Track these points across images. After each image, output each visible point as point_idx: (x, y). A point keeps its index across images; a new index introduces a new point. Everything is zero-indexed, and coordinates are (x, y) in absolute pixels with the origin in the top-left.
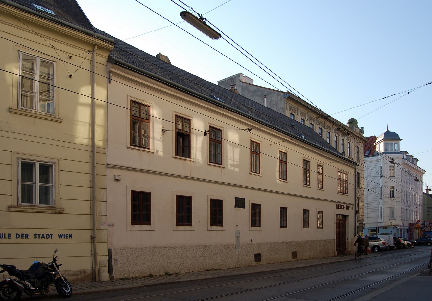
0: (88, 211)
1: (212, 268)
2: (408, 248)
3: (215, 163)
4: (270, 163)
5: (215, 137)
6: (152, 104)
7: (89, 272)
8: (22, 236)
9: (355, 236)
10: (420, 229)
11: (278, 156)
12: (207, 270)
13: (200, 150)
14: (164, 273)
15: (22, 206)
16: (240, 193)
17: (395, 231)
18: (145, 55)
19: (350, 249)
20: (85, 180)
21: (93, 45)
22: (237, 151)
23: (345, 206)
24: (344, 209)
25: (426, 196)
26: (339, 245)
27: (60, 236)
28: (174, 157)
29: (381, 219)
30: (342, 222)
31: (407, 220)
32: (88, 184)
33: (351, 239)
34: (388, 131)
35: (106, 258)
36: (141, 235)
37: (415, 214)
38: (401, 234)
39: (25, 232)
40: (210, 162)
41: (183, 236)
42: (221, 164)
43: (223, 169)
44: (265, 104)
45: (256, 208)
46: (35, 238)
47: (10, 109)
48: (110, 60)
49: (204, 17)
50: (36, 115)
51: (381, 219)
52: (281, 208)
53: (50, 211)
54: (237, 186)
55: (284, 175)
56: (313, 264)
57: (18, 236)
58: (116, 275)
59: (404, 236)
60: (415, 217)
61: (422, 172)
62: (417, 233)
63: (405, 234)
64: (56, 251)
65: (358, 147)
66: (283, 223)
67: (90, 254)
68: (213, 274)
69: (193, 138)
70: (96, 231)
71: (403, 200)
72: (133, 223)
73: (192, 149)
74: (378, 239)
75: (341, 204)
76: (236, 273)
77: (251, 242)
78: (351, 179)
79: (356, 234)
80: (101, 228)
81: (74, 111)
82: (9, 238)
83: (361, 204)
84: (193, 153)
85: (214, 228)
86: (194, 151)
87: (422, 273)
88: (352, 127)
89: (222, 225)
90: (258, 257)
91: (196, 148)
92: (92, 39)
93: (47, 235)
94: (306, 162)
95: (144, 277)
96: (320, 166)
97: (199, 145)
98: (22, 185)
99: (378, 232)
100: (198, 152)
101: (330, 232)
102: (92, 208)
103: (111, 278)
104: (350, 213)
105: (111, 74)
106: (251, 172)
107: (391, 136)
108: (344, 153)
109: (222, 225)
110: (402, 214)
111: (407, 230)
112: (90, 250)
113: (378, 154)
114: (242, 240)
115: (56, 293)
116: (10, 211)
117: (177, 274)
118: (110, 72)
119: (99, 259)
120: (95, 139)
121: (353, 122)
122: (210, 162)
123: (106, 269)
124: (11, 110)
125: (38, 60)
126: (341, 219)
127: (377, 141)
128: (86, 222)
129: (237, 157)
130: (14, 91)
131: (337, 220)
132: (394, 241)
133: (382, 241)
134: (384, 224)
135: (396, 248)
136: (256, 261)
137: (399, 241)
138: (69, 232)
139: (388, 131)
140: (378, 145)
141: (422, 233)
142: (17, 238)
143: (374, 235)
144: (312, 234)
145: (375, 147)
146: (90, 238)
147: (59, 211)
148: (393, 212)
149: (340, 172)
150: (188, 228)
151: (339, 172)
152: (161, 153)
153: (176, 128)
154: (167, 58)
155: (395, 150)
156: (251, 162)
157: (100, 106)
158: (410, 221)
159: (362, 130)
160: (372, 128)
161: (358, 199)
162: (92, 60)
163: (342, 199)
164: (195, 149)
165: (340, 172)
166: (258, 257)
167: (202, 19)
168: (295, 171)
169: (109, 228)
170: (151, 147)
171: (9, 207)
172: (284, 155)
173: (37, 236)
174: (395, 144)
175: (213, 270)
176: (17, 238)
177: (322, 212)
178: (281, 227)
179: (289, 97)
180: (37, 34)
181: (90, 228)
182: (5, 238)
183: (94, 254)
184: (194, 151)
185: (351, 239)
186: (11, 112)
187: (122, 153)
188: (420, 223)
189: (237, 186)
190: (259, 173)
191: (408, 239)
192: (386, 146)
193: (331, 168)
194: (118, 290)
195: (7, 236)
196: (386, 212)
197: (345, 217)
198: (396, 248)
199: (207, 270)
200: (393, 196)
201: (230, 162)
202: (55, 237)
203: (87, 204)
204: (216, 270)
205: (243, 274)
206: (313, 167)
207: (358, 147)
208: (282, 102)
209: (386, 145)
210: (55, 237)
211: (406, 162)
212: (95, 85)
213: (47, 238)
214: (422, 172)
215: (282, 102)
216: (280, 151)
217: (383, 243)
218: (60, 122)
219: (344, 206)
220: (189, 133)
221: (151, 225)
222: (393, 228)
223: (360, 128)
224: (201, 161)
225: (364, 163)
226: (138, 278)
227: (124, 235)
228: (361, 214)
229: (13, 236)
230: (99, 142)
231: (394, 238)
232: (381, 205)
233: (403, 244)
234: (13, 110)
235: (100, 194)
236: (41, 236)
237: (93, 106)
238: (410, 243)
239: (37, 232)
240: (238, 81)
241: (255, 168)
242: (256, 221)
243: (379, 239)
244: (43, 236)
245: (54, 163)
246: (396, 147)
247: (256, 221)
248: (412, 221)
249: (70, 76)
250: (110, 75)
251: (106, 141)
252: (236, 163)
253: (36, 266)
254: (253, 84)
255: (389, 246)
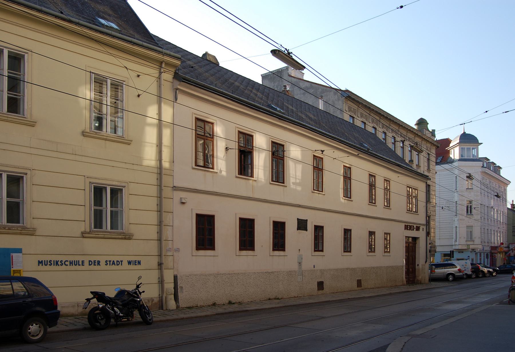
0: (155, 236)
1: (274, 297)
2: (489, 277)
3: (278, 182)
4: (333, 180)
5: (278, 153)
6: (216, 120)
7: (156, 300)
8: (94, 263)
9: (426, 262)
10: (504, 254)
11: (342, 172)
12: (269, 299)
13: (262, 168)
14: (227, 302)
15: (95, 232)
16: (303, 214)
17: (473, 256)
18: (195, 58)
19: (420, 277)
20: (153, 203)
21: (161, 63)
22: (300, 167)
23: (415, 227)
24: (413, 230)
25: (511, 212)
26: (407, 273)
27: (129, 263)
28: (237, 177)
29: (456, 241)
30: (411, 246)
31: (488, 243)
32: (155, 208)
33: (422, 265)
34: (464, 133)
35: (172, 285)
36: (204, 262)
37: (497, 234)
38: (480, 259)
39: (97, 258)
40: (272, 181)
41: (246, 262)
42: (283, 183)
43: (285, 188)
44: (321, 106)
45: (319, 230)
46: (106, 265)
47: (83, 132)
48: (177, 76)
49: (290, 51)
50: (108, 138)
51: (456, 241)
52: (345, 229)
53: (120, 237)
54: (299, 206)
55: (348, 193)
56: (381, 294)
57: (91, 263)
58: (182, 304)
59: (484, 262)
60: (497, 238)
61: (506, 183)
62: (500, 258)
63: (486, 260)
64: (140, 278)
65: (429, 154)
66: (347, 248)
67: (157, 282)
68: (278, 303)
69: (256, 155)
70: (163, 257)
71: (483, 218)
72: (198, 249)
73: (254, 167)
74: (453, 265)
75: (411, 225)
76: (302, 302)
77: (313, 269)
78: (422, 196)
79: (428, 260)
80: (168, 254)
81: (142, 132)
82: (83, 265)
83: (432, 223)
84: (255, 171)
85: (277, 253)
86: (257, 170)
87: (501, 303)
88: (419, 130)
89: (284, 250)
90: (321, 285)
91: (258, 166)
92: (160, 56)
93: (117, 261)
94: (372, 176)
95: (209, 306)
96: (387, 181)
97: (261, 161)
98: (94, 210)
99: (453, 257)
100: (260, 171)
101: (398, 258)
102: (160, 233)
103: (178, 307)
104: (421, 234)
105: (178, 91)
106: (314, 190)
107: (468, 140)
108: (413, 161)
109: (284, 250)
110: (481, 235)
111: (487, 255)
112: (158, 277)
113: (452, 161)
114: (304, 267)
115: (141, 320)
116: (83, 237)
117: (240, 303)
118: (177, 89)
119: (166, 286)
120: (163, 161)
121: (422, 123)
122: (272, 181)
123: (172, 297)
124: (84, 134)
125: (109, 82)
126: (410, 242)
127: (451, 145)
128: (153, 248)
129: (299, 174)
130: (86, 114)
131: (406, 243)
132: (472, 268)
133: (458, 268)
134: (460, 247)
135: (474, 276)
136: (319, 289)
137: (478, 268)
138: (137, 259)
139: (464, 133)
140: (452, 151)
141: (507, 258)
142: (90, 265)
143: (447, 260)
144: (379, 260)
145: (448, 152)
146: (157, 264)
147: (128, 237)
148: (471, 232)
149: (410, 188)
150: (250, 253)
151: (408, 187)
152: (224, 173)
153: (239, 146)
154: (214, 57)
155: (473, 155)
156: (314, 179)
157: (167, 126)
158: (491, 243)
159: (433, 133)
160: (444, 129)
161: (428, 218)
162: (159, 78)
163: (411, 219)
164: (257, 167)
165: (410, 188)
166: (321, 285)
167: (289, 53)
168: (360, 188)
169: (175, 253)
170: (215, 168)
171: (82, 233)
172: (347, 170)
173: (108, 262)
174: (473, 149)
175: (275, 299)
176: (90, 265)
177: (389, 234)
178: (344, 252)
179: (349, 97)
180: (111, 54)
181: (157, 254)
182: (79, 265)
183: (161, 282)
184: (257, 170)
185: (422, 265)
186: (84, 135)
187: (188, 176)
188: (504, 245)
189: (299, 206)
190: (322, 192)
191: (489, 266)
192: (462, 151)
193: (400, 182)
194: (192, 318)
195: (80, 263)
196: (463, 232)
197: (415, 239)
198: (474, 276)
199: (269, 299)
200: (471, 213)
201: (292, 180)
202: (125, 263)
203: (155, 229)
204: (278, 299)
205: (309, 303)
206: (380, 184)
207: (429, 154)
208: (340, 102)
209: (462, 150)
210: (125, 263)
211: (487, 171)
212: (163, 104)
213: (117, 265)
214: (506, 183)
215: (340, 102)
216: (344, 166)
217: (459, 270)
218: (129, 144)
219: (413, 226)
220: (251, 150)
221: (214, 250)
222: (471, 252)
223: (431, 130)
224: (263, 180)
225: (436, 173)
226: (203, 306)
227: (189, 262)
228: (432, 234)
229: (86, 263)
230: (166, 164)
231: (472, 264)
232: (456, 224)
233: (483, 272)
234: (87, 134)
235: (167, 218)
236: (111, 263)
237: (160, 125)
238: (491, 270)
239: (109, 258)
240: (287, 75)
241: (318, 185)
242: (318, 244)
243: (454, 265)
244: (114, 263)
245: (124, 187)
246: (474, 152)
247: (318, 244)
248: (494, 243)
249: (139, 96)
250: (176, 93)
251: (172, 162)
252: (298, 181)
253: (121, 293)
254: (305, 79)
255: (466, 274)
